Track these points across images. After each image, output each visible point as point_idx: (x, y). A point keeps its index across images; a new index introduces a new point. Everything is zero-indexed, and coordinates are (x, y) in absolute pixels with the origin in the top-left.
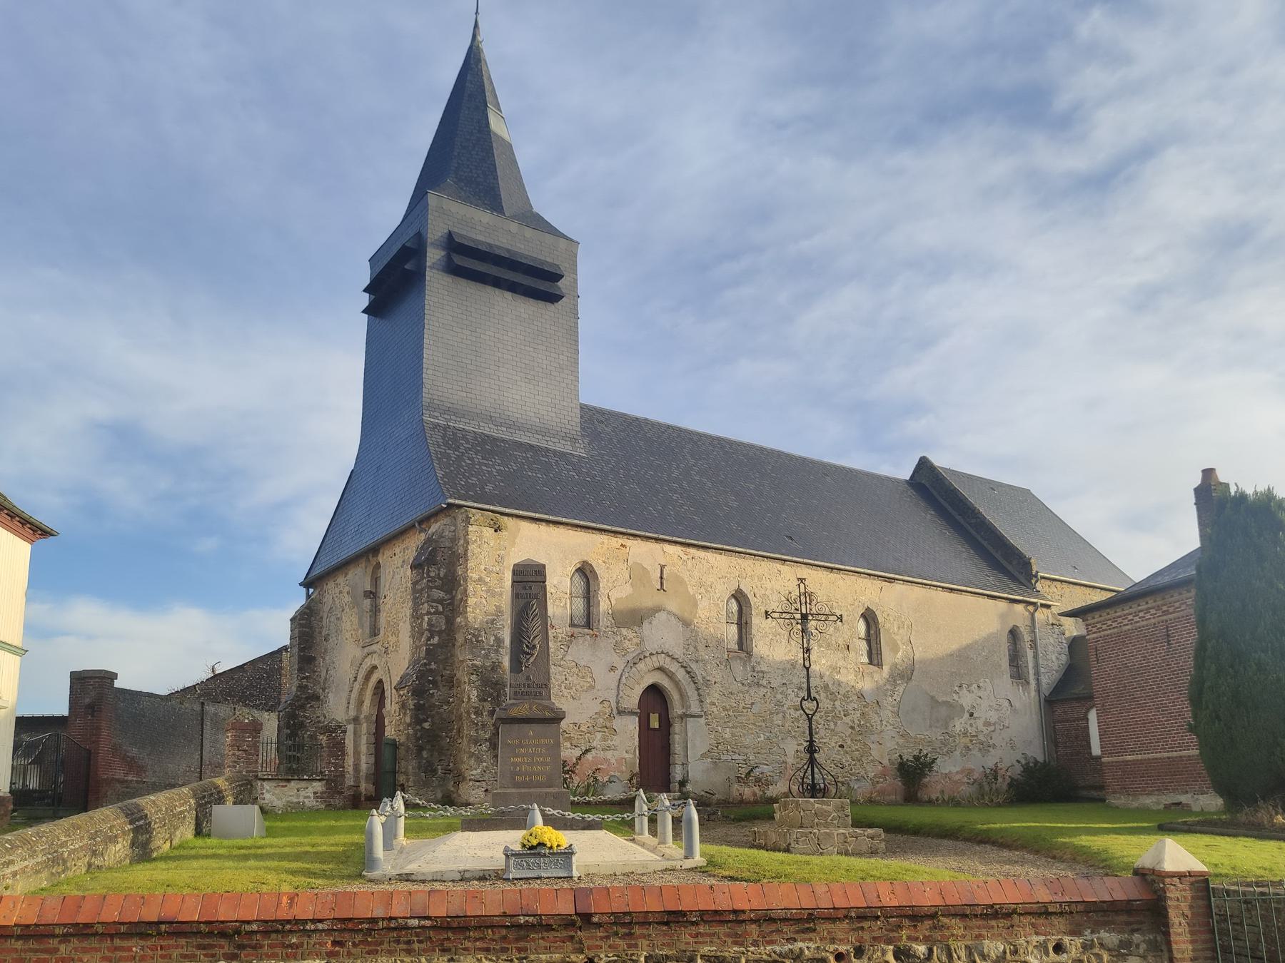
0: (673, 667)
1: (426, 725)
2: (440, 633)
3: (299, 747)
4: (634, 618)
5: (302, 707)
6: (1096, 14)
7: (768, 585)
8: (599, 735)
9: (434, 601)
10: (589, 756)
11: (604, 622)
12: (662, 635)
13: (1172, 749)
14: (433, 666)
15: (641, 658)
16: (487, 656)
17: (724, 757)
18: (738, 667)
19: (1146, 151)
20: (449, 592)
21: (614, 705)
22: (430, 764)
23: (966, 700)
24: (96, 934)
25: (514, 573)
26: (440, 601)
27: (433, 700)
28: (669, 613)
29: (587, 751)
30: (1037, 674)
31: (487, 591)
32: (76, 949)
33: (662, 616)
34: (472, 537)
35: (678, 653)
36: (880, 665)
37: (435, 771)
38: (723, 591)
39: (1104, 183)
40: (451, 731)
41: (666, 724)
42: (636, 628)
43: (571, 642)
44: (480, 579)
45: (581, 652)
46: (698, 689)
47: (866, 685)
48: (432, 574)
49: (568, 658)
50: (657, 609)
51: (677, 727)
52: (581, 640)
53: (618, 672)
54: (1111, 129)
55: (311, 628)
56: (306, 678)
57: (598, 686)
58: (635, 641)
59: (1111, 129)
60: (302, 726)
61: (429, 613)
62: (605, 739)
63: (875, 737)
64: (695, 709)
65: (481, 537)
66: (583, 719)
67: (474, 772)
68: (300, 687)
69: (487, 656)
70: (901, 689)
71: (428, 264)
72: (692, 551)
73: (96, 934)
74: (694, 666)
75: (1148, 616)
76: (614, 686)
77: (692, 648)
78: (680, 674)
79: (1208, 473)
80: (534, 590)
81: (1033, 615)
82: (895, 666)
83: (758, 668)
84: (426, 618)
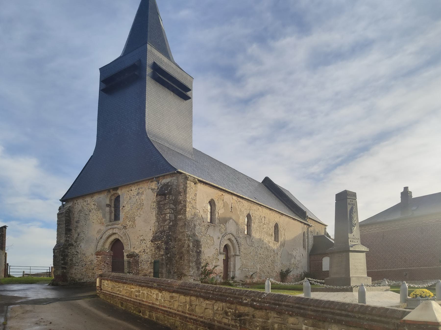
0: (233, 239)
1: (169, 255)
2: (173, 221)
3: (65, 263)
4: (225, 221)
5: (67, 248)
6: (255, 46)
7: (256, 213)
8: (215, 261)
9: (171, 209)
10: (217, 268)
11: (217, 221)
12: (231, 227)
14: (170, 233)
15: (226, 234)
16: (191, 230)
17: (244, 269)
18: (248, 239)
19: (262, 94)
20: (175, 206)
21: (219, 251)
22: (169, 270)
23: (294, 253)
26: (173, 209)
27: (170, 246)
28: (233, 220)
29: (216, 266)
30: (308, 246)
33: (231, 221)
34: (188, 185)
35: (235, 234)
36: (278, 241)
37: (171, 272)
39: (247, 102)
40: (176, 258)
44: (190, 202)
45: (211, 232)
46: (239, 247)
47: (275, 247)
48: (170, 198)
49: (207, 233)
50: (230, 218)
51: (232, 259)
52: (211, 227)
53: (220, 239)
54: (253, 85)
55: (70, 218)
56: (68, 237)
59: (253, 85)
60: (67, 256)
61: (169, 213)
63: (276, 264)
64: (238, 253)
65: (190, 185)
66: (211, 255)
67: (191, 273)
68: (66, 241)
69: (191, 230)
70: (282, 249)
71: (147, 74)
72: (239, 199)
75: (375, 230)
76: (219, 244)
78: (235, 241)
79: (406, 188)
80: (353, 203)
81: (308, 229)
82: (281, 242)
84: (168, 215)
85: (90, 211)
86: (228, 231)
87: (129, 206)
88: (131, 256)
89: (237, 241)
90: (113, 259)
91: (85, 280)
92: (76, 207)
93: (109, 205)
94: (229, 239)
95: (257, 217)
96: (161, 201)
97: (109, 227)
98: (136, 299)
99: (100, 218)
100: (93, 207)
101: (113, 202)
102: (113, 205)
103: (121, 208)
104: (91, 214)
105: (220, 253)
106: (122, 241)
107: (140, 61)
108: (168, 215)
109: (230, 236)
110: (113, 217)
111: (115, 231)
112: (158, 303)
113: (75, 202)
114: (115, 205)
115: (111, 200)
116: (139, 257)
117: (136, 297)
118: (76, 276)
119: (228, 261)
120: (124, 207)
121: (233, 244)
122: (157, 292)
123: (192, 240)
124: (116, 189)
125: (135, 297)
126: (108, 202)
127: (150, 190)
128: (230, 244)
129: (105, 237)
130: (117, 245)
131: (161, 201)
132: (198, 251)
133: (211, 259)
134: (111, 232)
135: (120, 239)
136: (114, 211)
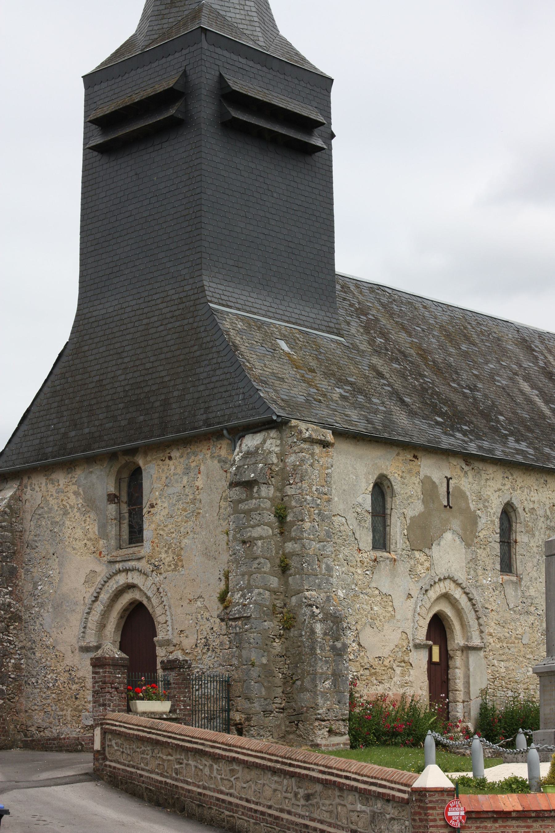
0: (457, 594)
13: (135, 441)
24: (531, 817)
25: (410, 519)
31: (319, 514)
32: (541, 826)
35: (461, 577)
38: (496, 507)
41: (446, 655)
42: (427, 551)
43: (374, 567)
46: (478, 618)
49: (373, 585)
51: (458, 661)
52: (383, 565)
57: (398, 617)
58: (427, 564)
62: (403, 674)
64: (476, 641)
65: (312, 455)
66: (385, 652)
67: (320, 711)
73: (531, 817)
74: (474, 591)
77: (472, 572)
78: (463, 601)
83: (527, 594)
85: (66, 513)
86: (441, 571)
87: (166, 505)
88: (170, 665)
89: (470, 600)
90: (128, 677)
91: (55, 731)
92: (28, 497)
93: (115, 496)
94: (446, 597)
95: (541, 512)
96: (240, 501)
97: (118, 566)
98: (176, 780)
99: (93, 537)
100: (73, 500)
101: (124, 486)
102: (124, 498)
103: (145, 511)
104: (68, 523)
105: (417, 646)
106: (150, 609)
107: (185, 74)
108: (259, 543)
109: (447, 587)
110: (125, 535)
111: (134, 578)
112: (212, 786)
113: (25, 481)
114: (130, 495)
115: (119, 481)
116: (189, 667)
117: (177, 774)
118: (30, 717)
119: (448, 667)
120: (152, 506)
121: (459, 612)
122: (211, 763)
123: (320, 616)
124: (133, 451)
125: (174, 775)
126: (112, 489)
127: (216, 462)
128: (449, 612)
129: (105, 597)
130: (137, 623)
131: (240, 501)
132: (339, 645)
133: (386, 663)
134: (121, 580)
135: (145, 602)
136: (127, 515)
